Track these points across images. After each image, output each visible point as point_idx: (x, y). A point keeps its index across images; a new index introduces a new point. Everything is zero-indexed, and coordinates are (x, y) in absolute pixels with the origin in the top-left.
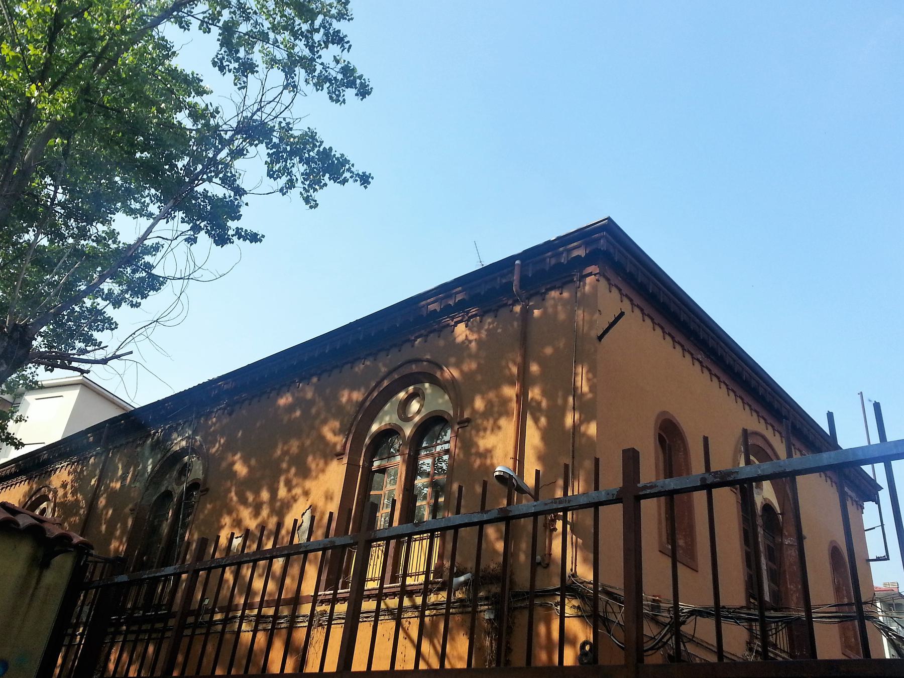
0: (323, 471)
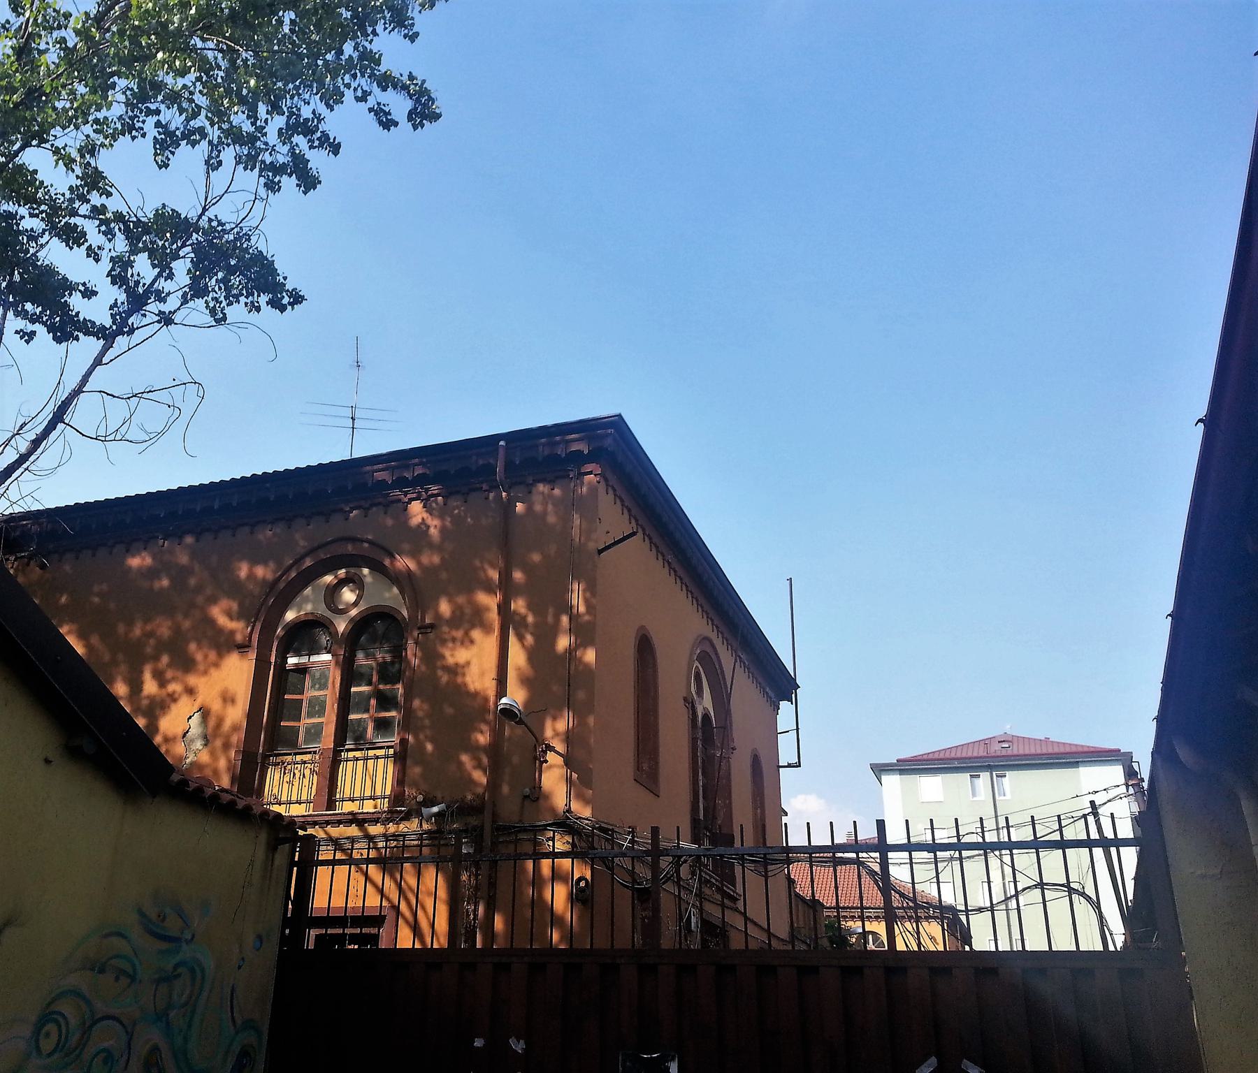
0: (216, 665)
